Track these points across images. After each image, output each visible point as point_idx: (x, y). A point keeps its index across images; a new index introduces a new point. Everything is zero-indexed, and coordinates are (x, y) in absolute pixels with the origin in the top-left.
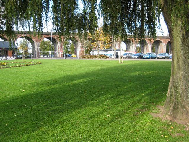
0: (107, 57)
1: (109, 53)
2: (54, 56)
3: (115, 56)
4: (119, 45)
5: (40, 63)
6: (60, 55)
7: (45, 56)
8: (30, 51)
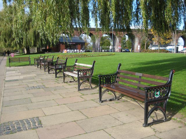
0: (167, 52)
1: (168, 48)
2: (113, 50)
3: (175, 51)
4: (177, 41)
5: (114, 55)
6: (118, 50)
7: (103, 51)
8: (58, 65)
